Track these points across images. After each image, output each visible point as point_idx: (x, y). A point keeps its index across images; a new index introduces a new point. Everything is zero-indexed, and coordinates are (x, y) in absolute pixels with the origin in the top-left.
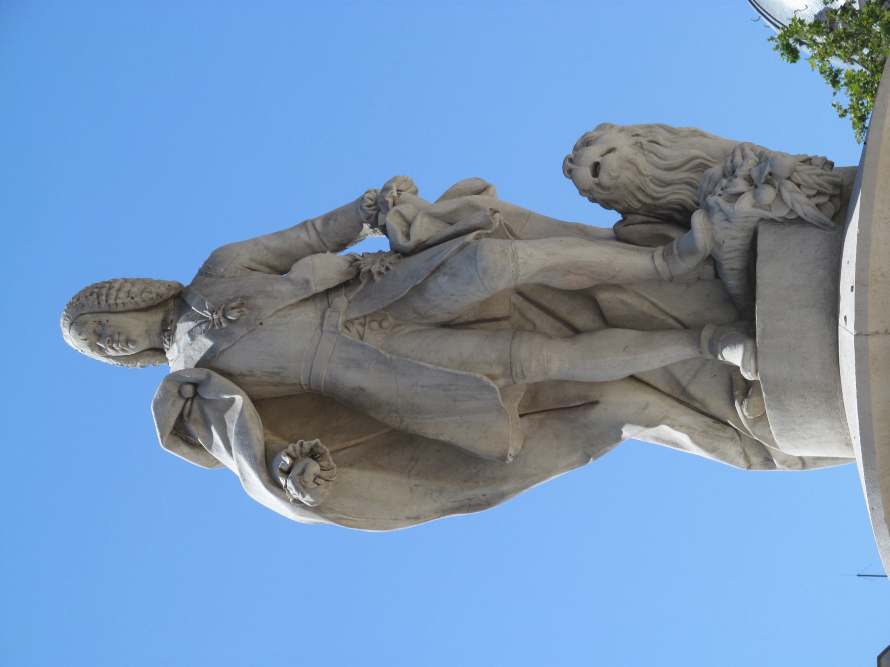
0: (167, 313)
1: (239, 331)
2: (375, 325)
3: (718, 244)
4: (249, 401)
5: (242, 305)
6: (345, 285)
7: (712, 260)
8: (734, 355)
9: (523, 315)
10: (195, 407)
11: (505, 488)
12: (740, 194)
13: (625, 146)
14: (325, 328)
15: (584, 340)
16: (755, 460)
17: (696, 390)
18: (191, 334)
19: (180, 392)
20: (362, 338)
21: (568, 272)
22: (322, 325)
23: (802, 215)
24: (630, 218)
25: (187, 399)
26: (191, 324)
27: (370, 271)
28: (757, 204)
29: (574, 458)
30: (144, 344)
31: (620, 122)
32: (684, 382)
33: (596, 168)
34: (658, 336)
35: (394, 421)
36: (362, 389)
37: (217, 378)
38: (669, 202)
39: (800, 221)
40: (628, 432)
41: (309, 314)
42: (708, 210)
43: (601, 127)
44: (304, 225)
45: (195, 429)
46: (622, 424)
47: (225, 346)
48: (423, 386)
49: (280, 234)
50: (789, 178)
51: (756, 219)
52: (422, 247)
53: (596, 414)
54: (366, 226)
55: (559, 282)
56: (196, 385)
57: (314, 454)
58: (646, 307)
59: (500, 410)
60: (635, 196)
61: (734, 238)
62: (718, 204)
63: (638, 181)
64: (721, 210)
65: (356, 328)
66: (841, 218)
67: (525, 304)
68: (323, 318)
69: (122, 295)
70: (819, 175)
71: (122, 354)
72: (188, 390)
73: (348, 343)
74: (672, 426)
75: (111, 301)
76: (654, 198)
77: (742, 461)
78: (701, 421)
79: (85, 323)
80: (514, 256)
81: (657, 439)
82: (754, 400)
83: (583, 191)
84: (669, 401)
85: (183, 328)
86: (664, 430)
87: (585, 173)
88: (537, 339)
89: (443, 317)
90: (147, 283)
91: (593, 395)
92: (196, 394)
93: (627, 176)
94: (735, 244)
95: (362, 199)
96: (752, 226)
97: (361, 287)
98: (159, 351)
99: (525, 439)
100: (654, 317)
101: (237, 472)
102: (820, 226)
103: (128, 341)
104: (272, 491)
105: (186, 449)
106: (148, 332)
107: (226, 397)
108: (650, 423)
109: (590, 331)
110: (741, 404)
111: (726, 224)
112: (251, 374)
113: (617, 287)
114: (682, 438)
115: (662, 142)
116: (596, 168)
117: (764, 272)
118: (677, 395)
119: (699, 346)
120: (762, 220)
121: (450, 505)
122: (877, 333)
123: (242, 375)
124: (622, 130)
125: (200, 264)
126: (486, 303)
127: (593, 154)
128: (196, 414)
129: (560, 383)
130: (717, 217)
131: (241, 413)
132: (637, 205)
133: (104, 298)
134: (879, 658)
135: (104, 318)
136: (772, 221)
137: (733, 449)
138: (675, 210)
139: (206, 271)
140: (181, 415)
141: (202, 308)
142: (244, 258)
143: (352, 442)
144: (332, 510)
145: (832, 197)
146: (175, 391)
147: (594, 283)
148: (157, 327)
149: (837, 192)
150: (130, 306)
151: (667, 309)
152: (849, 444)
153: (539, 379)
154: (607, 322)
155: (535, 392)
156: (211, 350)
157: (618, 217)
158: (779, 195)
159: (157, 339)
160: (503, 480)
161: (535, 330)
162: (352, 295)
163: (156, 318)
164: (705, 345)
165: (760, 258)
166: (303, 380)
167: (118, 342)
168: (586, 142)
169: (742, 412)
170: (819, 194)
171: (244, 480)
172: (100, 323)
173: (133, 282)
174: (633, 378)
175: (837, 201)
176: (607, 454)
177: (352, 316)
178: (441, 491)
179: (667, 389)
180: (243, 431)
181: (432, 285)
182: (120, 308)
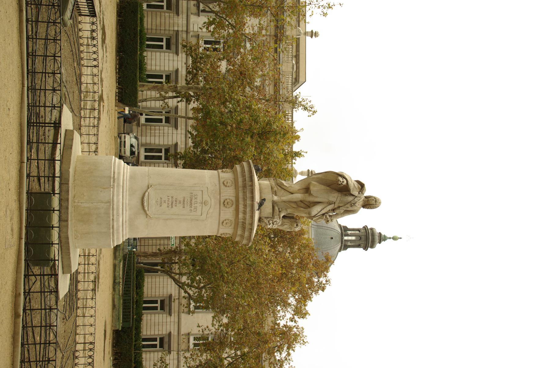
15: (299, 200)
154: (295, 202)
174: (292, 194)
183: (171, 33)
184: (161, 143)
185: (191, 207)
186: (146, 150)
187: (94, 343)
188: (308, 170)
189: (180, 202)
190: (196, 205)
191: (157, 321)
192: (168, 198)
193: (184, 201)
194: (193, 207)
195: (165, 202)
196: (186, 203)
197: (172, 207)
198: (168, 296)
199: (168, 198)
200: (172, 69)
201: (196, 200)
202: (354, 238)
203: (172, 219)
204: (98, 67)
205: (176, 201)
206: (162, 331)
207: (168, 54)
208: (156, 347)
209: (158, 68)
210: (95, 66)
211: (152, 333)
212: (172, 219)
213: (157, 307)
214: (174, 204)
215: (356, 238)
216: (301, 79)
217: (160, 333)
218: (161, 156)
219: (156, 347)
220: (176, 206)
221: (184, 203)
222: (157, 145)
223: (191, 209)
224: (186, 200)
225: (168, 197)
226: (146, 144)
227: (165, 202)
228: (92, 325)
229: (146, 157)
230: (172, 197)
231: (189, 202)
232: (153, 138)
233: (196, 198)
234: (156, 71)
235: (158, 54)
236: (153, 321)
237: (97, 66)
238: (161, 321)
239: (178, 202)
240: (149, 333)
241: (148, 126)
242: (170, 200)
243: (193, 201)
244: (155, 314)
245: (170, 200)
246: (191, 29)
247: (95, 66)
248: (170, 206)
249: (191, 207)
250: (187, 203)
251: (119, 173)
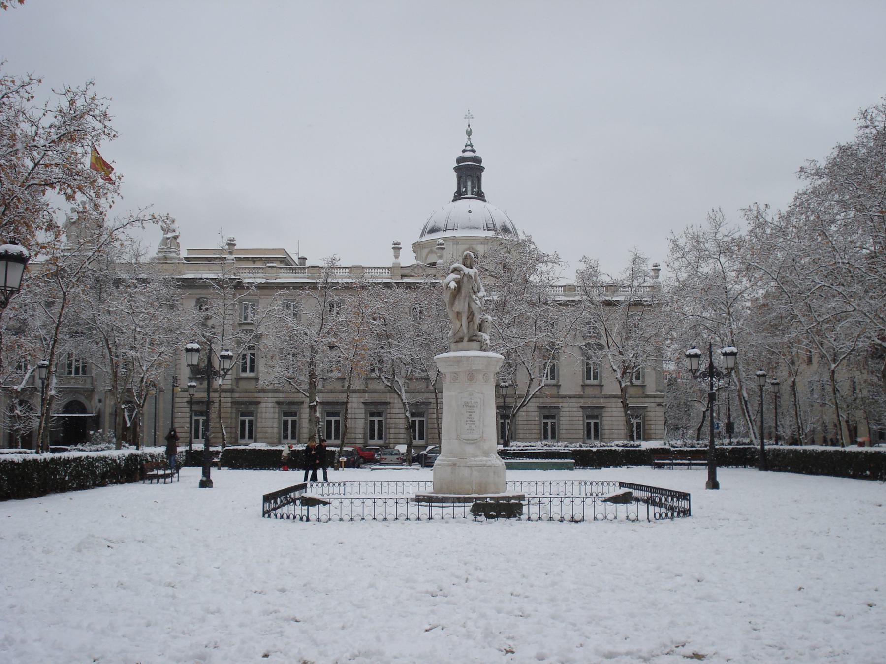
55: (474, 318)
183: (234, 411)
185: (474, 407)
188: (393, 248)
189: (470, 415)
191: (567, 423)
193: (469, 412)
195: (470, 427)
198: (539, 410)
200: (277, 409)
202: (469, 184)
203: (483, 420)
206: (579, 415)
207: (258, 414)
208: (597, 423)
209: (275, 425)
211: (581, 427)
212: (483, 420)
213: (551, 422)
217: (581, 418)
219: (597, 423)
226: (365, 438)
227: (470, 427)
229: (380, 437)
230: (467, 421)
233: (467, 403)
234: (279, 428)
235: (259, 425)
236: (568, 427)
238: (568, 418)
240: (581, 432)
244: (559, 425)
246: (230, 387)
247: (345, 485)
249: (474, 407)
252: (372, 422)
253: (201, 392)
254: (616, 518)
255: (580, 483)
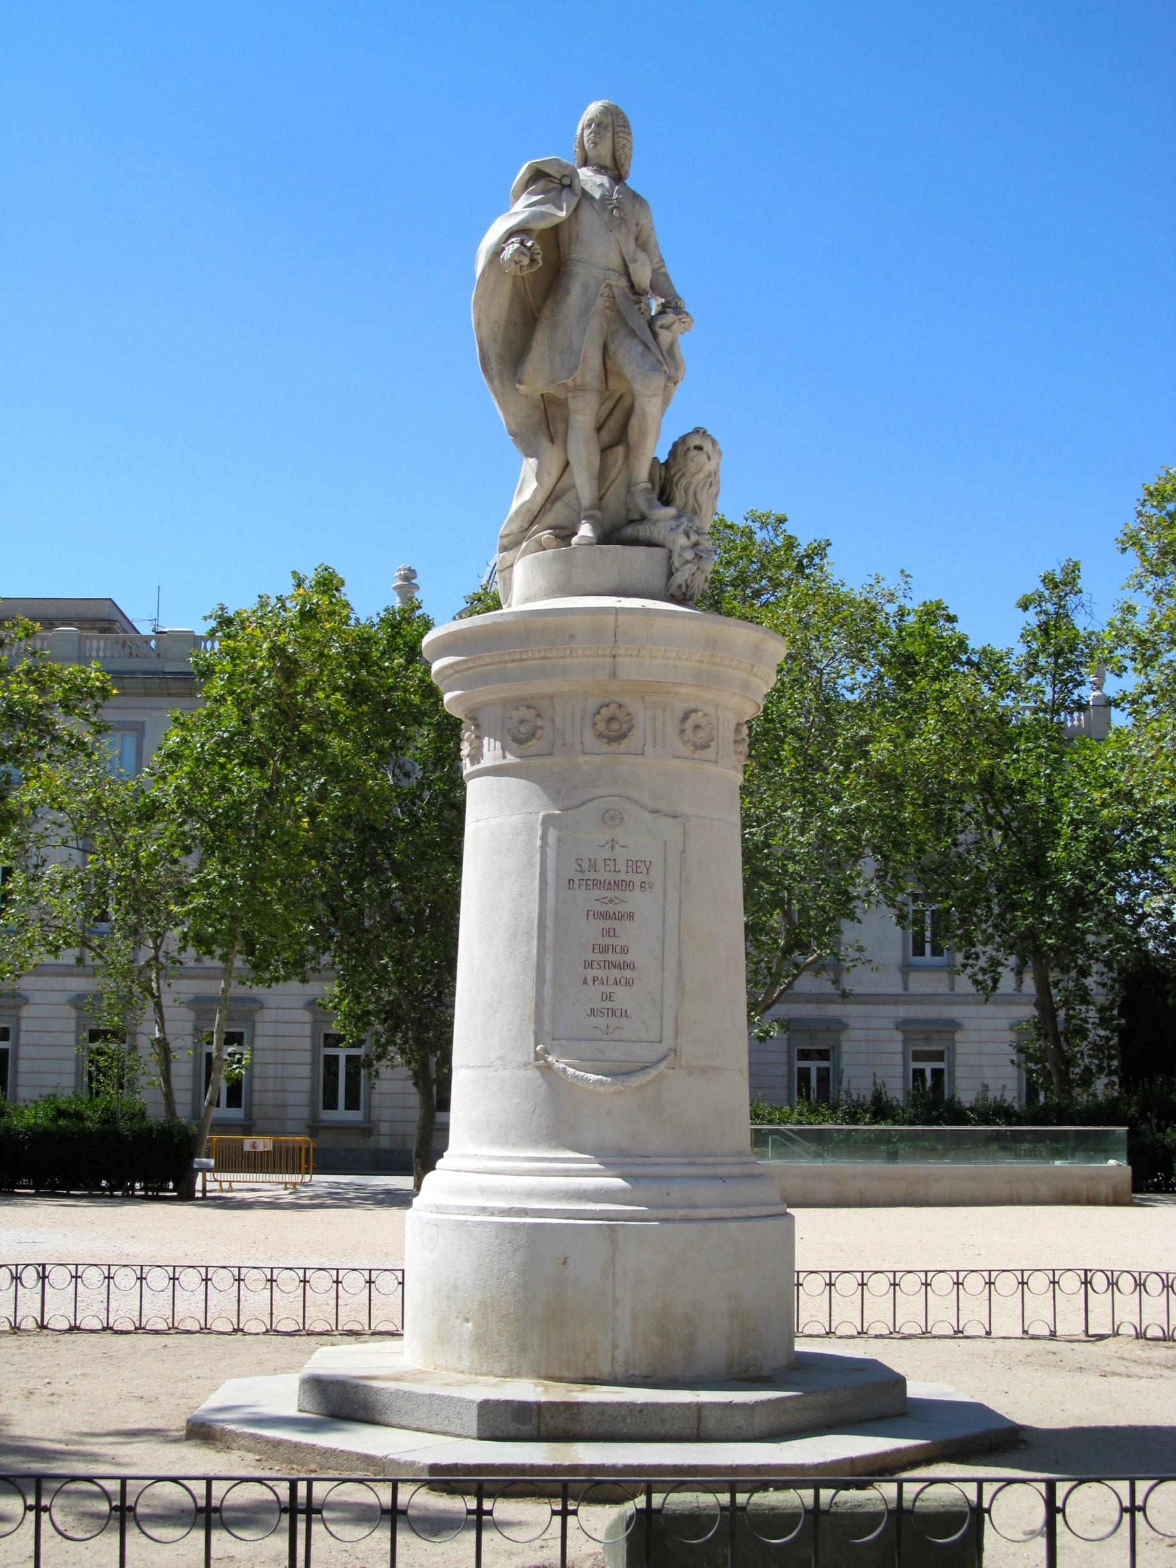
0: (611, 170)
1: (606, 216)
2: (608, 304)
3: (655, 523)
4: (562, 220)
5: (622, 219)
6: (632, 285)
7: (643, 519)
8: (585, 530)
9: (608, 398)
10: (556, 185)
11: (497, 383)
12: (688, 536)
13: (710, 467)
14: (608, 272)
15: (594, 436)
16: (506, 541)
17: (559, 505)
18: (601, 185)
19: (565, 176)
20: (602, 295)
21: (641, 428)
22: (609, 270)
23: (676, 575)
24: (663, 468)
25: (560, 180)
26: (607, 185)
27: (641, 302)
28: (683, 548)
29: (514, 427)
30: (591, 154)
31: (722, 463)
32: (564, 499)
33: (699, 448)
34: (595, 483)
35: (546, 312)
36: (568, 294)
37: (575, 201)
38: (674, 493)
39: (670, 574)
40: (532, 462)
41: (616, 262)
42: (678, 517)
43: (720, 453)
44: (662, 261)
45: (541, 184)
46: (538, 457)
47: (596, 206)
48: (571, 333)
49: (657, 245)
50: (698, 568)
51: (671, 546)
52: (655, 335)
53: (545, 442)
54: (663, 300)
55: (634, 422)
56: (570, 186)
57: (533, 261)
58: (613, 476)
59: (552, 382)
60: (678, 471)
61: (659, 533)
62: (682, 524)
63: (689, 473)
64: (678, 526)
65: (607, 292)
66: (672, 599)
67: (614, 400)
68: (613, 271)
69: (624, 141)
70: (698, 587)
71: (585, 139)
72: (566, 181)
73: (598, 288)
74: (536, 490)
75: (621, 134)
76: (677, 483)
77: (506, 532)
78: (536, 507)
79: (606, 115)
80: (655, 395)
81: (524, 480)
82: (554, 542)
83: (684, 439)
84: (551, 489)
85: (604, 180)
86: (534, 485)
87: (696, 441)
88: (596, 406)
89: (612, 347)
90: (629, 157)
91: (558, 441)
92: (564, 186)
93: (692, 467)
94: (655, 534)
95: (680, 299)
96: (667, 544)
97: (631, 296)
98: (585, 163)
99: (527, 396)
100: (605, 482)
101: (512, 211)
102: (667, 586)
103: (595, 143)
104: (505, 232)
105: (526, 178)
106: (600, 157)
107: (564, 206)
108: (538, 476)
109: (599, 438)
110: (550, 534)
111: (668, 529)
112: (577, 223)
113: (627, 456)
114: (527, 495)
115: (711, 490)
116: (699, 448)
117: (641, 551)
118: (554, 493)
119: (590, 509)
120: (671, 551)
121: (485, 346)
122: (616, 620)
123: (576, 217)
124: (718, 465)
125: (638, 192)
126: (620, 375)
127: (708, 447)
128: (551, 185)
129: (566, 421)
130: (673, 523)
131: (555, 215)
132: (672, 472)
133: (623, 129)
134: (110, 599)
135: (610, 129)
136: (670, 558)
137: (515, 527)
138: (669, 496)
139: (635, 197)
140: (549, 175)
141: (618, 192)
142: (644, 221)
143: (527, 286)
144: (490, 271)
145: (684, 594)
146: (566, 173)
147: (631, 444)
148: (602, 163)
149: (687, 598)
150: (617, 146)
151: (611, 489)
152: (527, 600)
153: (571, 407)
154: (605, 450)
155: (562, 404)
156: (593, 198)
157: (662, 461)
158: (687, 562)
159: (594, 162)
160: (501, 381)
161: (602, 405)
162: (626, 290)
163: (608, 162)
164: (591, 512)
165: (648, 549)
166: (573, 256)
167: (595, 137)
168: (714, 442)
169: (546, 535)
170: (687, 586)
171: (511, 215)
172: (607, 126)
173: (631, 149)
174: (567, 464)
175: (682, 597)
176: (515, 448)
177: (615, 290)
178: (495, 341)
179: (558, 487)
180: (543, 216)
181: (636, 341)
182: (616, 140)
184: (307, 1057)
185: (630, 885)
186: (331, 1104)
187: (1086, 1271)
189: (608, 933)
190: (621, 866)
192: (590, 980)
193: (604, 915)
194: (627, 877)
196: (611, 908)
197: (631, 966)
199: (590, 980)
201: (600, 866)
203: (680, 964)
204: (44, 1266)
205: (605, 949)
210: (43, 1277)
212: (680, 964)
214: (618, 958)
215: (29, 1494)
216: (105, 612)
218: (349, 1059)
220: (624, 950)
221: (614, 917)
222: (314, 1071)
223: (637, 885)
224: (599, 907)
225: (585, 982)
226: (312, 1106)
227: (609, 997)
228: (1054, 1282)
229: (353, 1103)
230: (588, 965)
231: (610, 894)
232: (291, 1085)
235: (23, 1065)
237: (40, 1269)
239: (609, 941)
241: (251, 1099)
242: (600, 973)
243: (602, 876)
245: (600, 973)
247: (43, 1277)
248: (628, 974)
249: (630, 885)
250: (611, 901)
251: (483, 1191)
252: (331, 1062)
253: (716, 1207)
254: (988, 1333)
255: (1086, 1283)
